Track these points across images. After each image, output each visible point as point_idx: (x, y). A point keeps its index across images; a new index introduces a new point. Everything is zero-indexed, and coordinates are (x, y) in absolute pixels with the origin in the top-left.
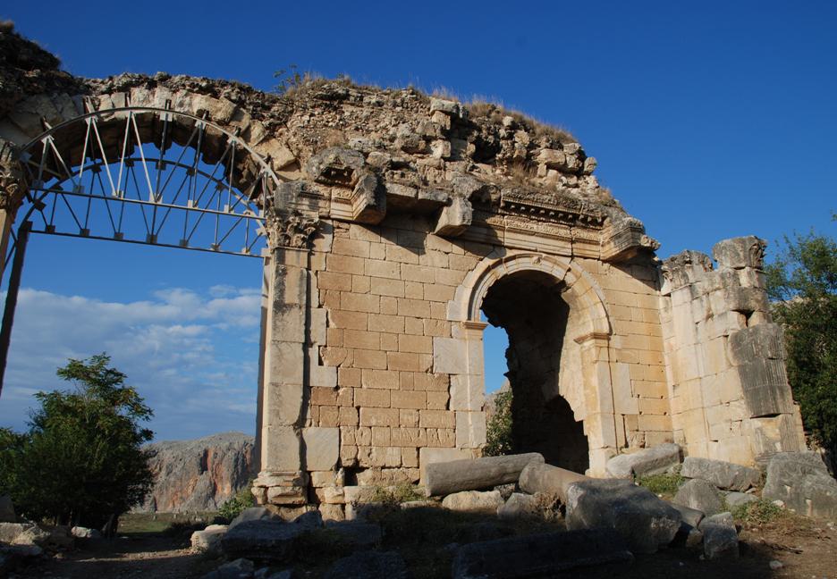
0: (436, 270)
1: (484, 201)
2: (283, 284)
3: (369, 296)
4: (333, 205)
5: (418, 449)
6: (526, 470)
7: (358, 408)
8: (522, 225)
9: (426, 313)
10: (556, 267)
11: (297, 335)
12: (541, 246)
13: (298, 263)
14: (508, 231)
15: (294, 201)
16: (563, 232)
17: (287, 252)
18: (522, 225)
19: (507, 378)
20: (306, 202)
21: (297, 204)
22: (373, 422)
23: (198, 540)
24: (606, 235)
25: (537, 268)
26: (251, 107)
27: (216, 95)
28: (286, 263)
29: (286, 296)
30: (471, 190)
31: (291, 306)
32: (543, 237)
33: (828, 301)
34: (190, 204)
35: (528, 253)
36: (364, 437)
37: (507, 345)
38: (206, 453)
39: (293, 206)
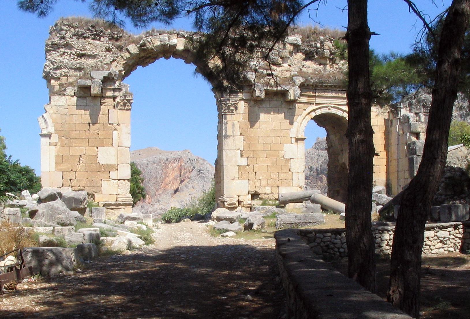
1: (306, 85)
3: (259, 129)
5: (278, 187)
7: (256, 173)
9: (282, 135)
11: (232, 147)
12: (332, 102)
17: (227, 115)
22: (261, 178)
24: (444, 140)
25: (330, 111)
26: (148, 34)
31: (229, 136)
36: (258, 183)
38: (25, 205)
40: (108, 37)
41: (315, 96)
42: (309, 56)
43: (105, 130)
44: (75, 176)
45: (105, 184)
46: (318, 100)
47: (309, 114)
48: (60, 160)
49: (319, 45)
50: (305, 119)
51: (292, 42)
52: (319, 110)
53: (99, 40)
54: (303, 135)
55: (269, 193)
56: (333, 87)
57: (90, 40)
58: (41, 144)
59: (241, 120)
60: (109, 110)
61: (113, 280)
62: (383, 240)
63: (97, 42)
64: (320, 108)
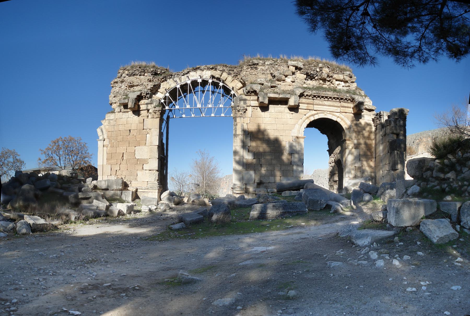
0: (288, 119)
2: (236, 128)
4: (251, 102)
6: (306, 184)
8: (321, 103)
10: (333, 116)
13: (241, 121)
14: (315, 105)
15: (239, 102)
16: (338, 104)
18: (321, 103)
19: (328, 152)
20: (242, 102)
21: (239, 103)
23: (169, 215)
27: (216, 70)
28: (237, 122)
29: (237, 132)
30: (300, 93)
32: (329, 106)
33: (63, 149)
34: (188, 106)
35: (323, 111)
37: (327, 140)
39: (238, 104)
40: (151, 73)
41: (313, 104)
42: (310, 77)
43: (141, 134)
44: (119, 167)
45: (140, 173)
46: (316, 107)
47: (308, 118)
48: (110, 156)
49: (318, 70)
50: (304, 122)
51: (294, 65)
52: (317, 115)
53: (144, 75)
54: (303, 135)
55: (272, 182)
56: (332, 98)
57: (138, 76)
58: (98, 147)
59: (249, 122)
60: (144, 119)
61: (92, 207)
62: (376, 9)
63: (142, 77)
64: (317, 114)
